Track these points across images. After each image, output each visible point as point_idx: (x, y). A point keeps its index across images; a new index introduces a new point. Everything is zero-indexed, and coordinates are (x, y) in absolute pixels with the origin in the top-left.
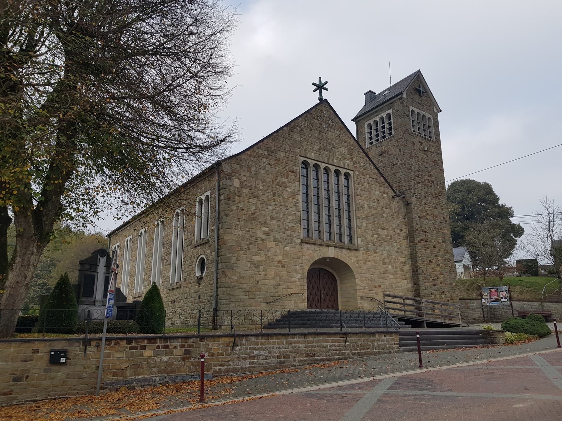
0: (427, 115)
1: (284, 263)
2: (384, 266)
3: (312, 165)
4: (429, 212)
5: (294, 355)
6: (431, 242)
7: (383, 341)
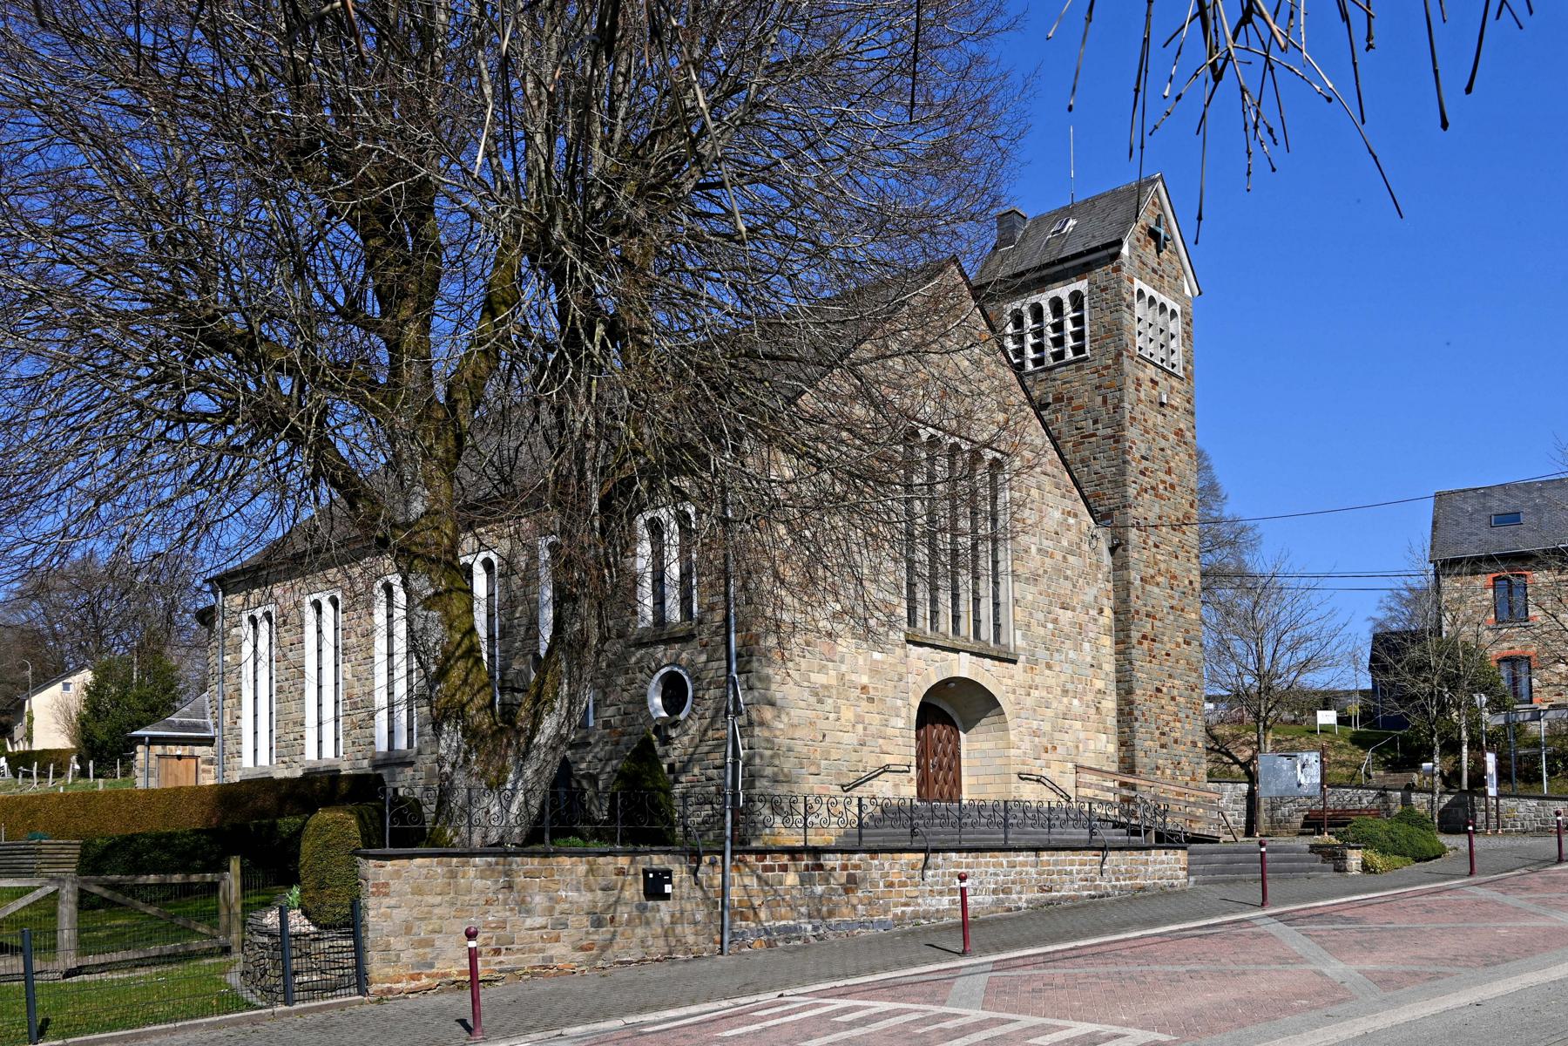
4: (1163, 566)
5: (1018, 888)
7: (1162, 862)
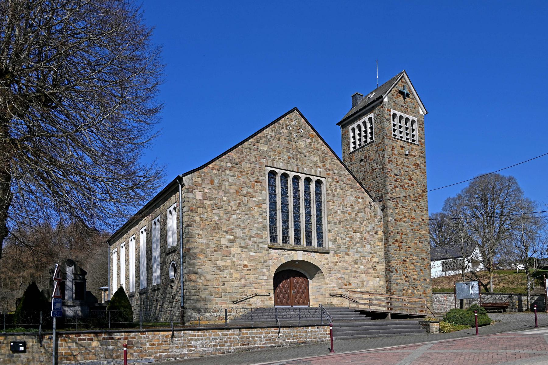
0: (411, 118)
1: (249, 267)
2: (356, 266)
3: (280, 175)
5: (229, 344)
6: (406, 243)
7: (316, 332)
